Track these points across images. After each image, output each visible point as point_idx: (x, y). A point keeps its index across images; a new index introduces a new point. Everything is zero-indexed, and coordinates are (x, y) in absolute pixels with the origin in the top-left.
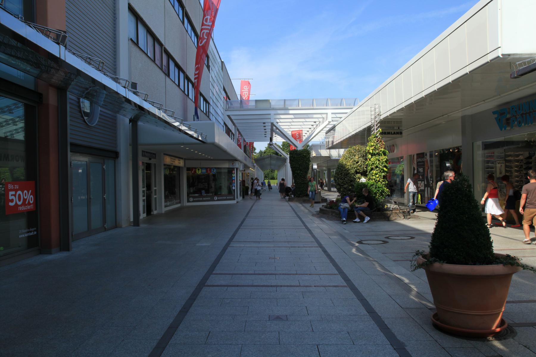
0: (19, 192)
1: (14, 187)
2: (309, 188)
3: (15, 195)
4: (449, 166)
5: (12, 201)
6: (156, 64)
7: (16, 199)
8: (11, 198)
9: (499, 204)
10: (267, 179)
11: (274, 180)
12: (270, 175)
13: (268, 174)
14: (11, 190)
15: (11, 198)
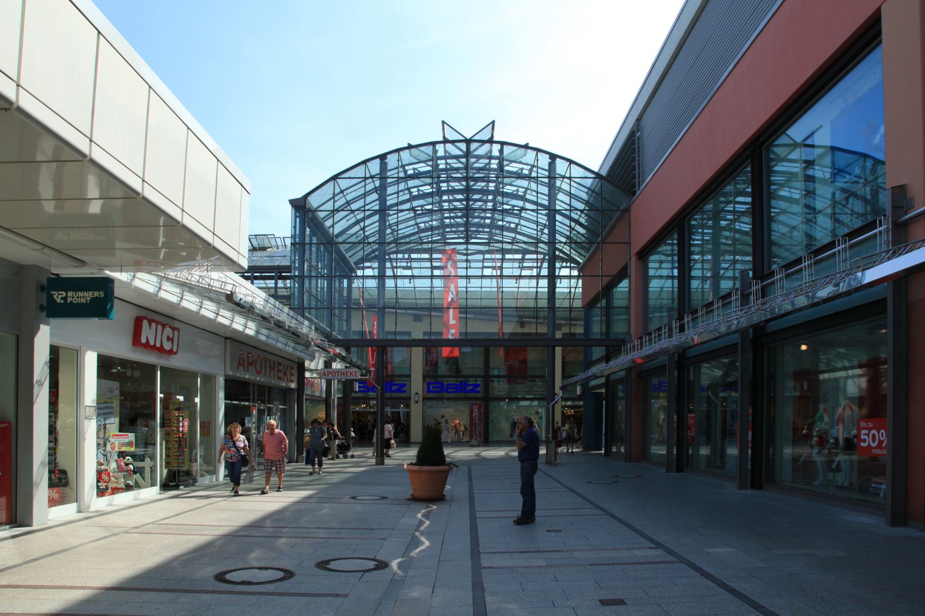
0: (874, 431)
1: (867, 425)
2: (339, 348)
3: (868, 435)
4: (182, 252)
5: (864, 441)
7: (869, 440)
8: (863, 437)
9: (68, 613)
14: (864, 428)
15: (863, 437)
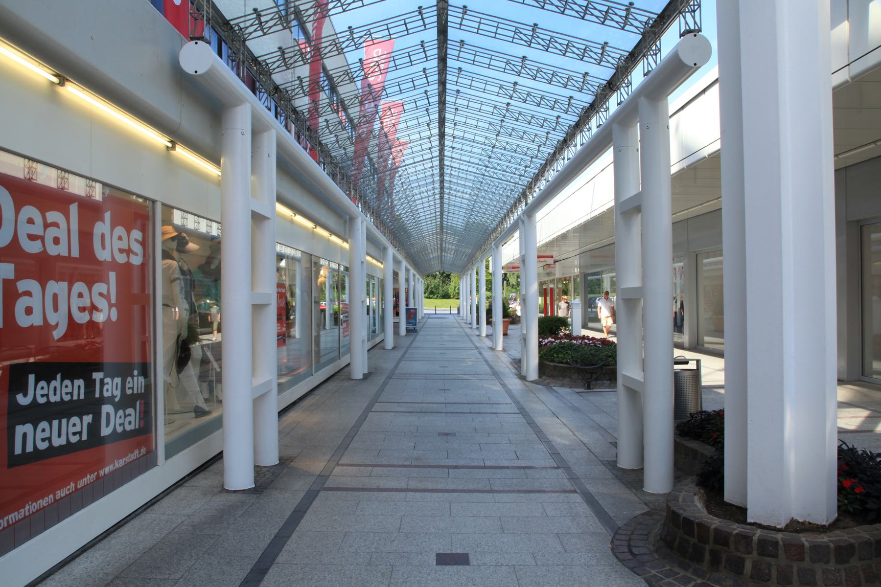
6: (384, 337)
10: (435, 296)
11: (449, 300)
12: (441, 288)
13: (437, 288)
